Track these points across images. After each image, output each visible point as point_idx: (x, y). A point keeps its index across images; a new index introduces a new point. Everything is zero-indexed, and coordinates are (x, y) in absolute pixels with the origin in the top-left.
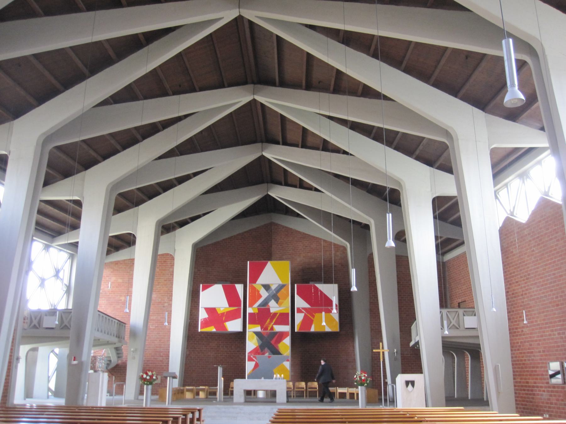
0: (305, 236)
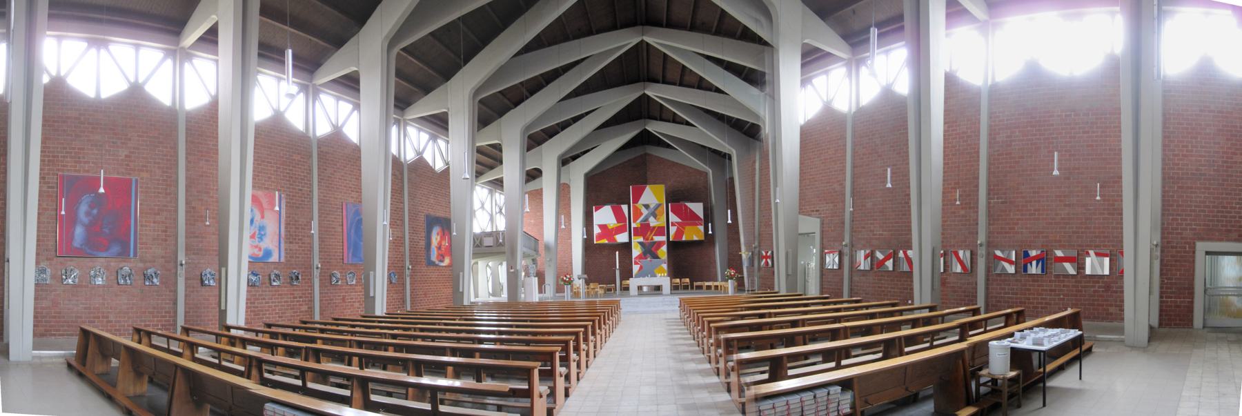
0: (674, 164)
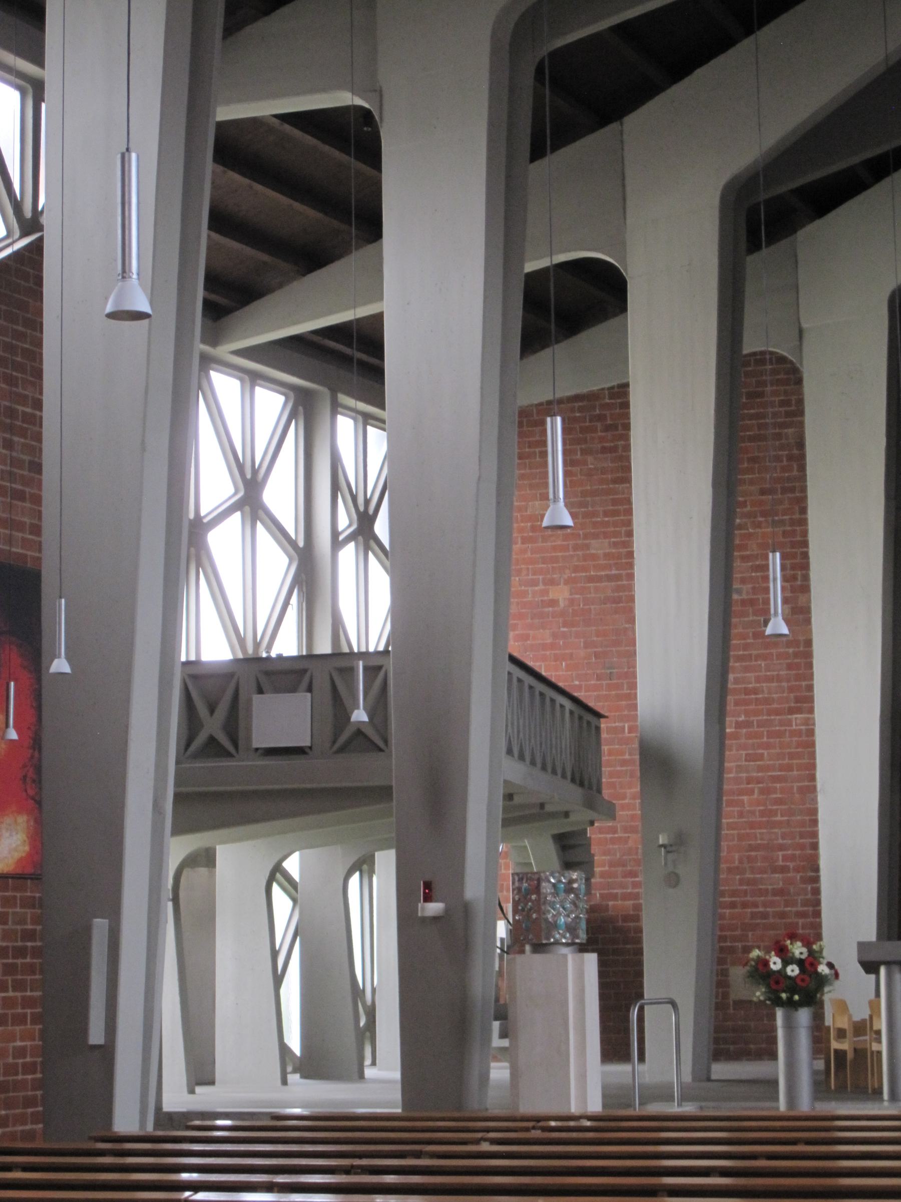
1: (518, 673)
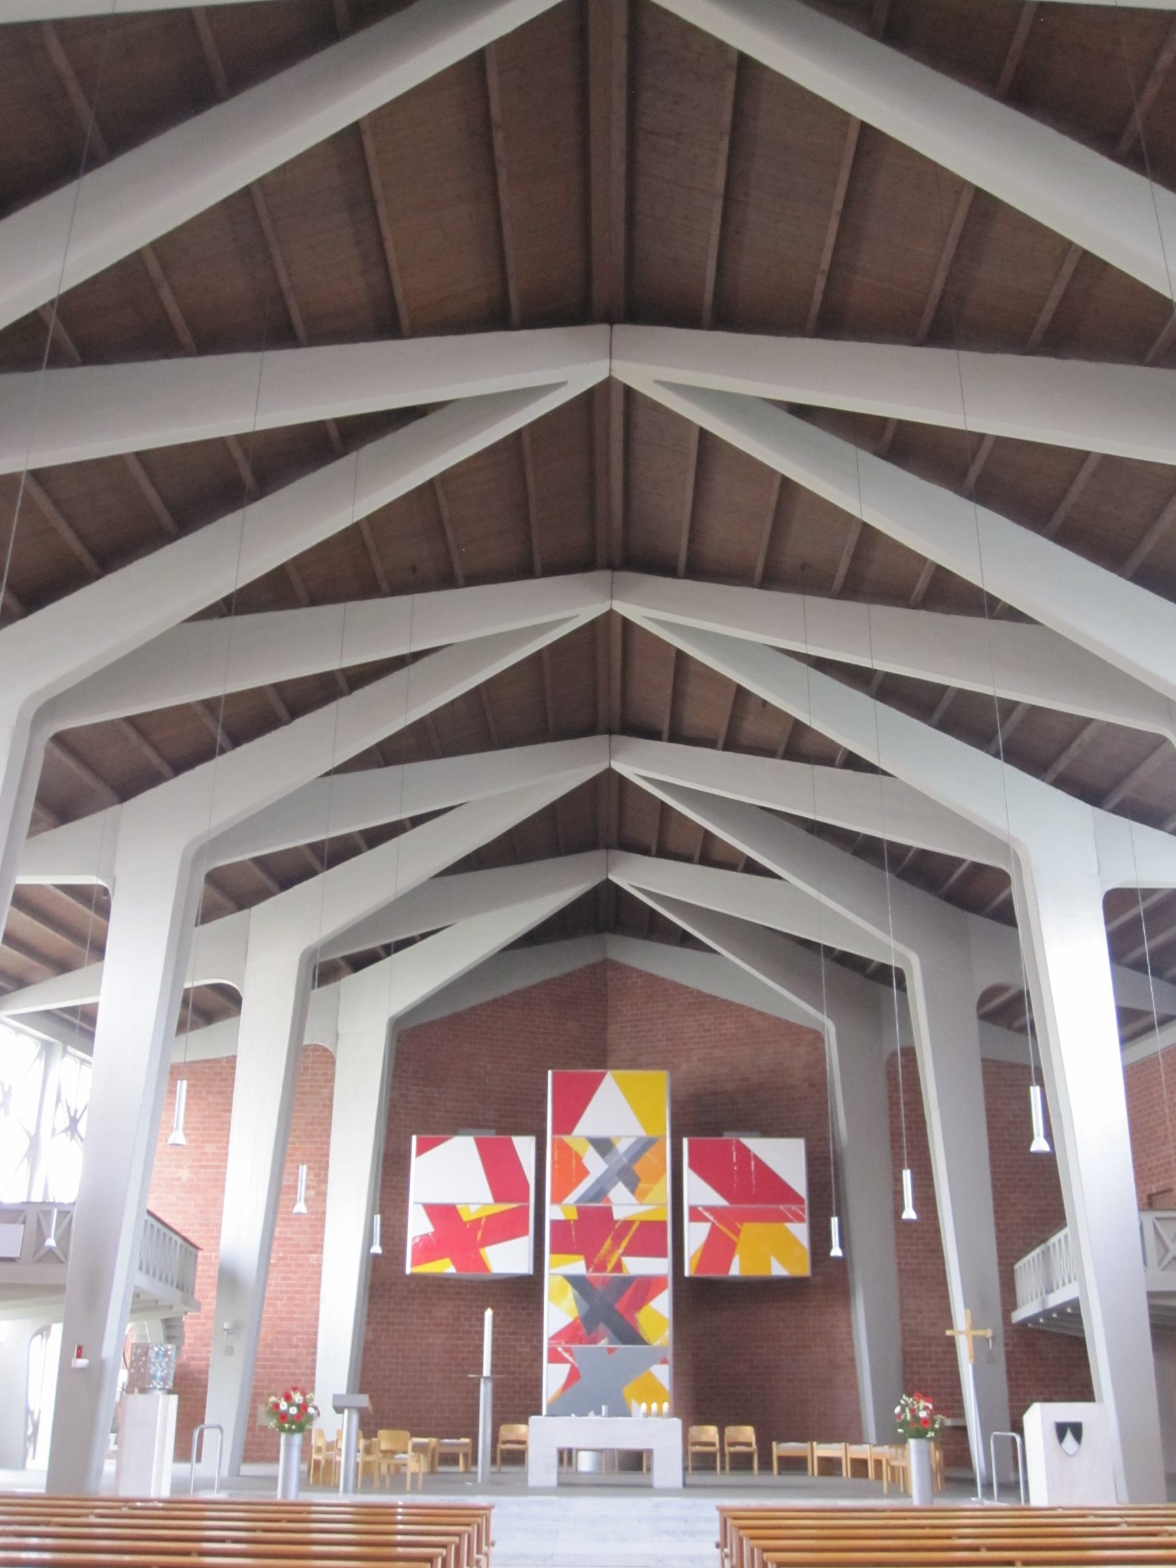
0: (704, 1002)
1: (151, 1220)
